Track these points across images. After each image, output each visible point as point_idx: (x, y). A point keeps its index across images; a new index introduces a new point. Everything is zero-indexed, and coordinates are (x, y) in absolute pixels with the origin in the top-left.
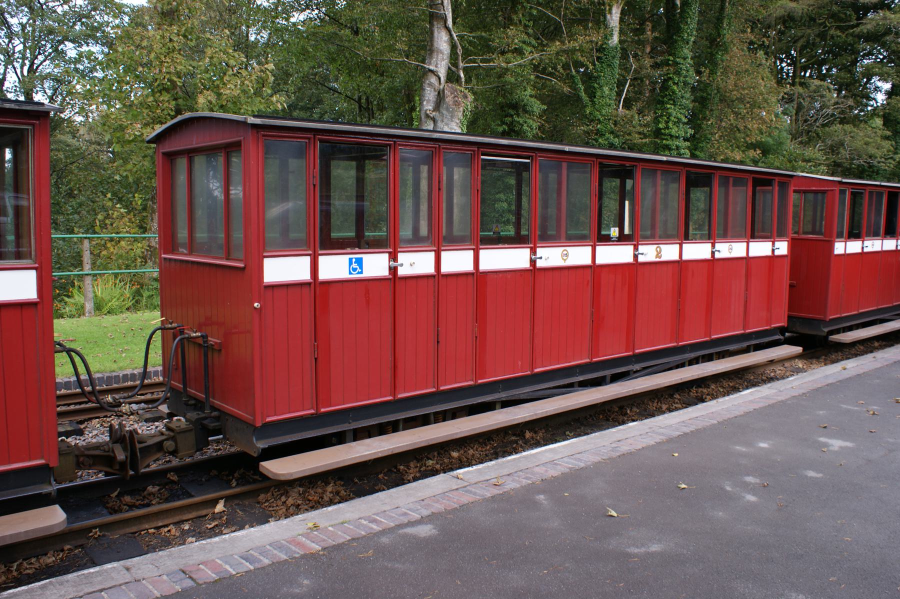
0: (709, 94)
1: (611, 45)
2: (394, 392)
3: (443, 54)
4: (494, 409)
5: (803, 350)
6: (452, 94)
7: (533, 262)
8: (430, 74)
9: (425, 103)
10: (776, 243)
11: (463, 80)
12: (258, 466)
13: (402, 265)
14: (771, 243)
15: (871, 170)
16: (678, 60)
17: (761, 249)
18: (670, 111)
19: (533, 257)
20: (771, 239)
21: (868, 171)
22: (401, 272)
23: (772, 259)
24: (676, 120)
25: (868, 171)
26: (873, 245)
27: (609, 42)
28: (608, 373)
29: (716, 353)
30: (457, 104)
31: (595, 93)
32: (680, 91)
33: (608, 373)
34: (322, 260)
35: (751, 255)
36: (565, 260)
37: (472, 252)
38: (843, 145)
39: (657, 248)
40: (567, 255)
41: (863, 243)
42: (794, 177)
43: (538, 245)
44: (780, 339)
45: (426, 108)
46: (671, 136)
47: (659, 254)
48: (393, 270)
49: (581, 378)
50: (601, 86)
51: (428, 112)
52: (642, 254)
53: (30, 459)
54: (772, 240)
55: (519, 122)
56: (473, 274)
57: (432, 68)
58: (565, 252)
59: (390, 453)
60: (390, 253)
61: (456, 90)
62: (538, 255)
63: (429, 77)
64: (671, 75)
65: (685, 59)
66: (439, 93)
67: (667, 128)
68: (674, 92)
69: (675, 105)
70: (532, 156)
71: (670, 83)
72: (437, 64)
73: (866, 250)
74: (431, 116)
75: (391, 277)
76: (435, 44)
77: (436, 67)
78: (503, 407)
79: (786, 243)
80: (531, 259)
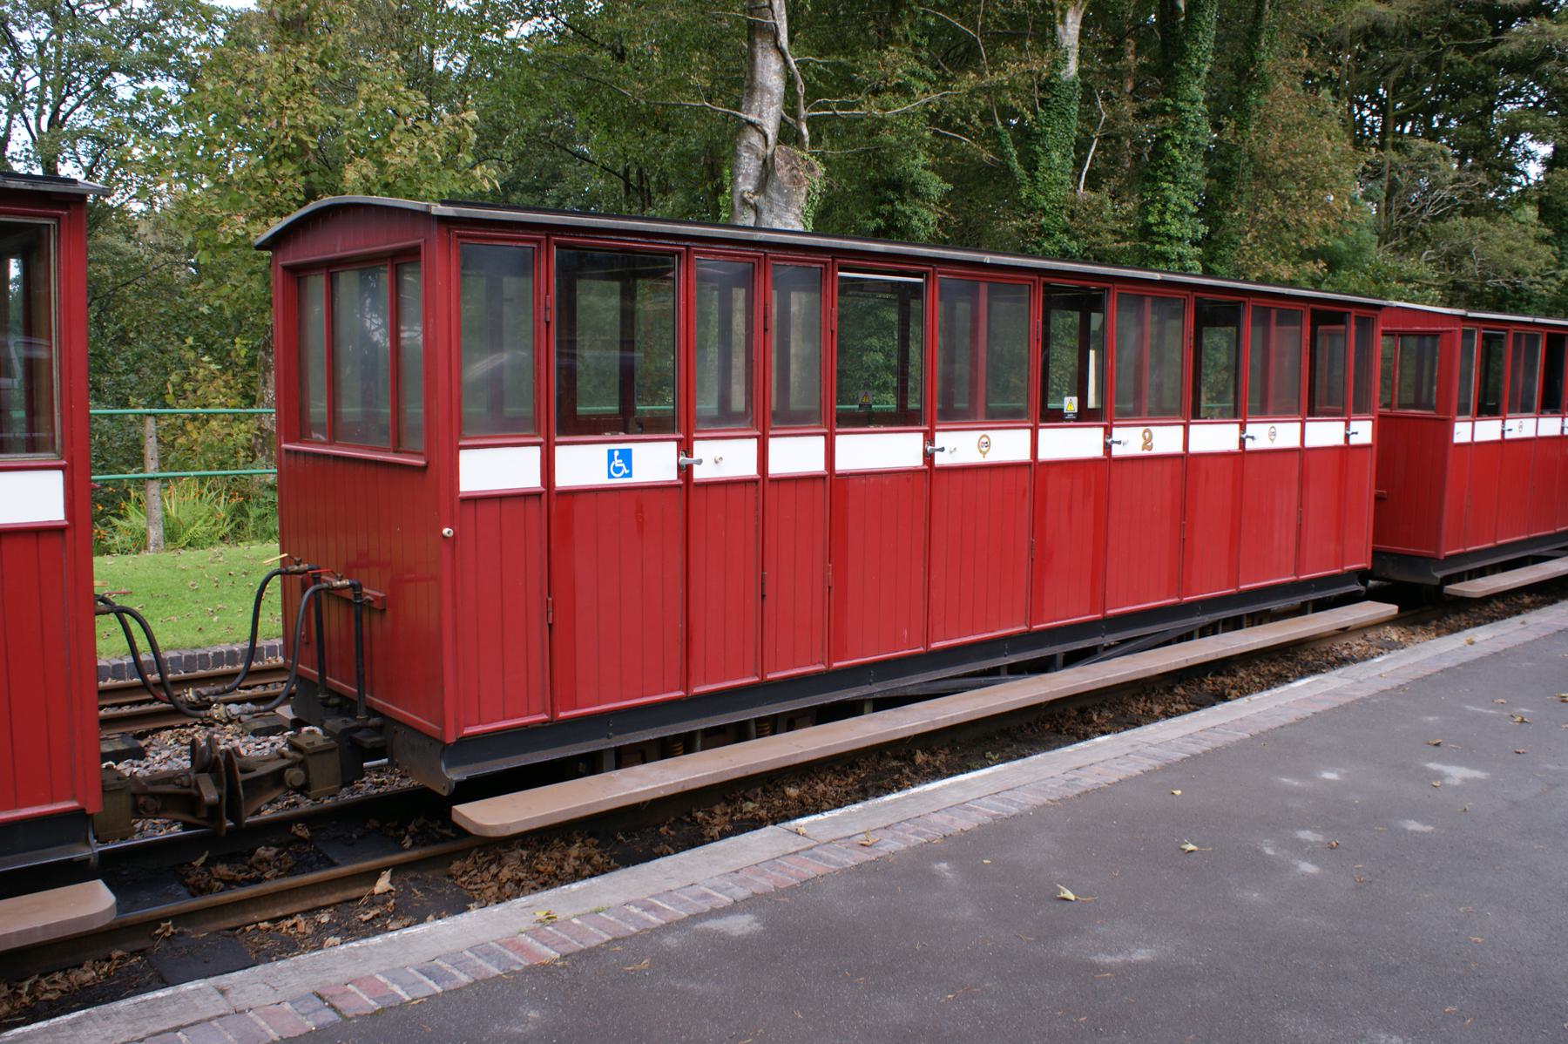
0: (1234, 165)
1: (1064, 79)
2: (686, 684)
3: (772, 94)
4: (861, 713)
5: (1400, 611)
6: (787, 163)
7: (929, 457)
8: (749, 128)
9: (740, 180)
10: (1353, 424)
11: (807, 139)
12: (449, 812)
13: (700, 462)
14: (1343, 424)
15: (1518, 296)
16: (1181, 104)
17: (1325, 433)
18: (1167, 193)
19: (929, 448)
20: (1343, 416)
21: (1513, 299)
22: (699, 474)
23: (1346, 451)
24: (1177, 209)
25: (1513, 299)
26: (1521, 427)
27: (1062, 73)
28: (1059, 650)
29: (1248, 615)
30: (796, 181)
31: (1037, 162)
32: (1184, 159)
33: (1059, 650)
34: (560, 452)
35: (1308, 444)
36: (984, 453)
37: (822, 440)
38: (1468, 252)
39: (1145, 432)
40: (988, 445)
41: (1503, 423)
42: (1383, 309)
43: (937, 427)
44: (1358, 591)
45: (742, 188)
46: (1170, 237)
47: (1147, 443)
48: (685, 471)
49: (1012, 659)
50: (1048, 151)
51: (746, 195)
52: (1119, 443)
53: (53, 800)
54: (1346, 418)
55: (904, 212)
56: (823, 477)
57: (752, 118)
58: (985, 440)
59: (679, 790)
60: (679, 441)
61: (794, 158)
62: (938, 445)
63: (748, 134)
64: (1169, 131)
65: (1193, 102)
66: (765, 161)
67: (1163, 223)
68: (1174, 161)
69: (1176, 184)
70: (927, 272)
71: (1168, 144)
72: (761, 111)
73: (1508, 436)
74: (752, 201)
75: (681, 483)
76: (758, 77)
77: (760, 116)
78: (875, 710)
79: (1370, 423)
80: (925, 451)
